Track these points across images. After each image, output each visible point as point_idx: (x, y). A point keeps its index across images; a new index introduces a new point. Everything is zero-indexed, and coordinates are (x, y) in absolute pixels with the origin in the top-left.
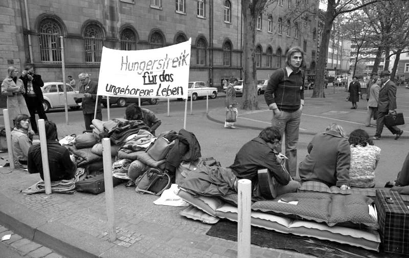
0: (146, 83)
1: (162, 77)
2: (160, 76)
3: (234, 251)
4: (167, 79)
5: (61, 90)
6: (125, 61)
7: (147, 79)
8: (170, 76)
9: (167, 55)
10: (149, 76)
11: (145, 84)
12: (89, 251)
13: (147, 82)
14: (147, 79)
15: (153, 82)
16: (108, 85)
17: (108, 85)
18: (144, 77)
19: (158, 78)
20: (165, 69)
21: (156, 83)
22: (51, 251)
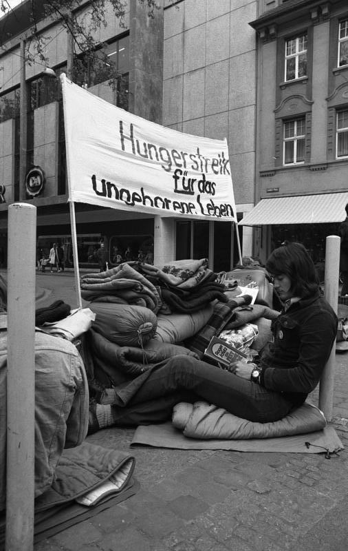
0: (178, 189)
1: (201, 184)
2: (200, 182)
3: (39, 390)
4: (208, 189)
5: (167, 201)
6: (127, 132)
7: (180, 182)
8: (211, 184)
9: (198, 149)
10: (184, 179)
11: (176, 191)
12: (9, 495)
13: (180, 187)
14: (180, 182)
15: (188, 191)
16: (94, 178)
17: (94, 178)
18: (176, 178)
19: (195, 185)
20: (204, 172)
21: (193, 193)
22: (198, 428)
